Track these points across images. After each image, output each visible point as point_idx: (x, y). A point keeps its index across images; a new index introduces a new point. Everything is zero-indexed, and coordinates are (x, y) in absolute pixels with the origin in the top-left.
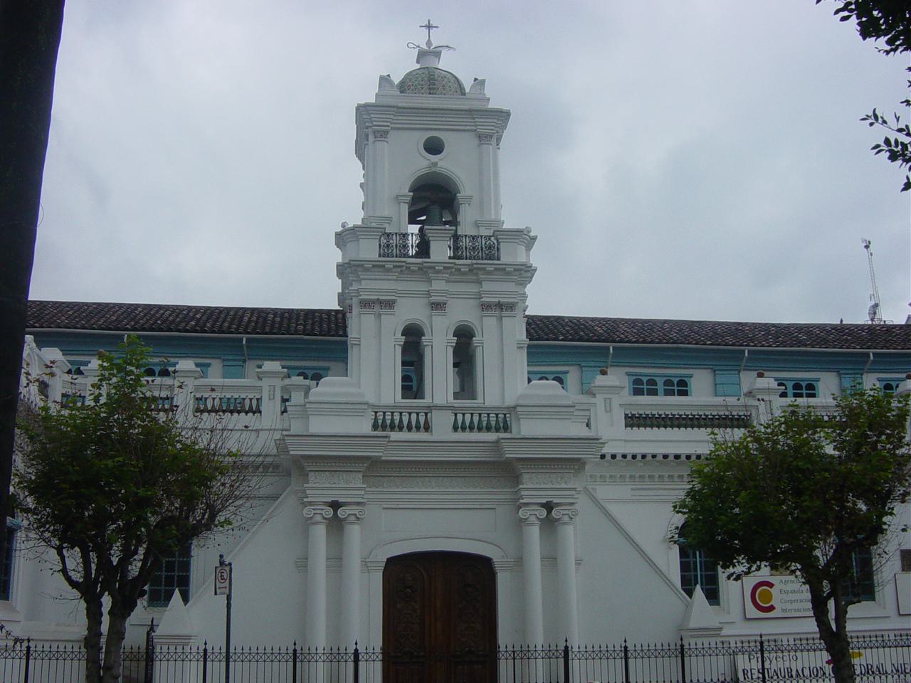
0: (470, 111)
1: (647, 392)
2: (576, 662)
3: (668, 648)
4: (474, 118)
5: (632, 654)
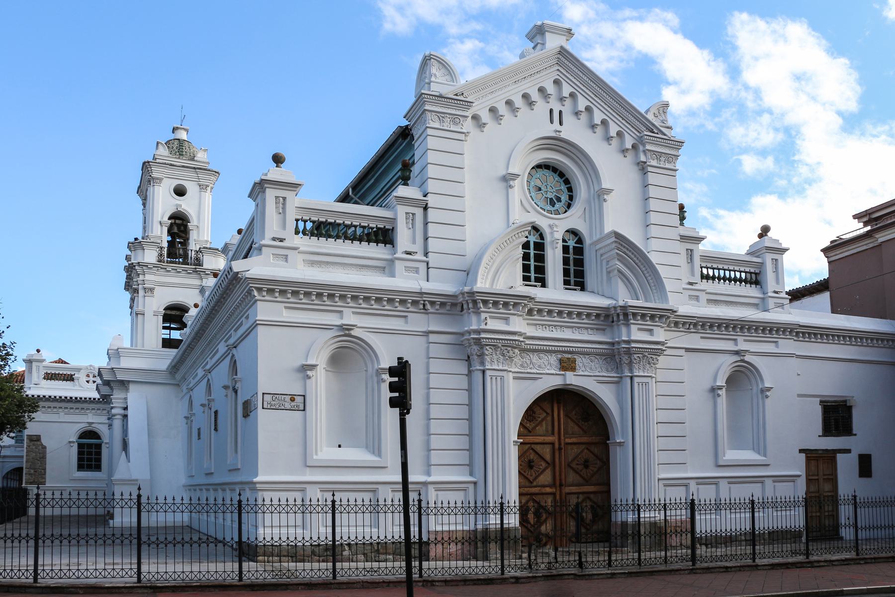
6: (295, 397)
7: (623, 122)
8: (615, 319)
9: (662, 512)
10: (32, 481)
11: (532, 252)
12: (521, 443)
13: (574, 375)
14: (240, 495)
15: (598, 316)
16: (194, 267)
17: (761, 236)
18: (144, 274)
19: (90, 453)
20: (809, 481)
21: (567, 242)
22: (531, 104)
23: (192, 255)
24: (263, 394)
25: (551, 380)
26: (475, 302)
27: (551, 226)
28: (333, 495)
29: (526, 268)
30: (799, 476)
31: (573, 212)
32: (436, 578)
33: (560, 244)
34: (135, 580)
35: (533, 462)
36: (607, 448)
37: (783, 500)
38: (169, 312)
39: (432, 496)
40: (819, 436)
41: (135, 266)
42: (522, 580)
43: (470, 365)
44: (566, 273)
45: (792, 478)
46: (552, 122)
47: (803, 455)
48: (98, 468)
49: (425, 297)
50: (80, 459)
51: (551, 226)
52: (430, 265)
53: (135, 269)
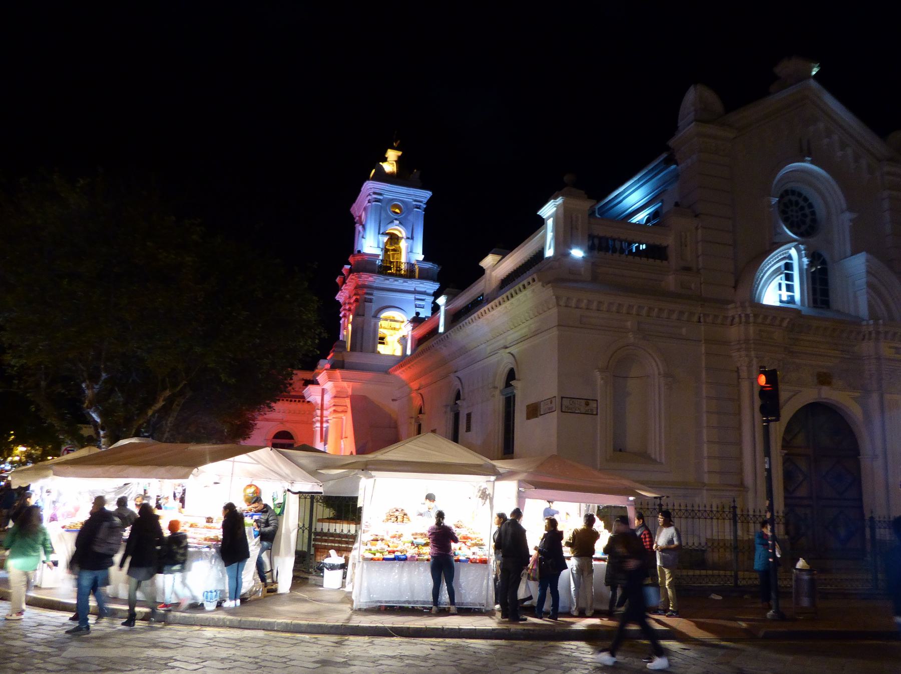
24: (562, 398)
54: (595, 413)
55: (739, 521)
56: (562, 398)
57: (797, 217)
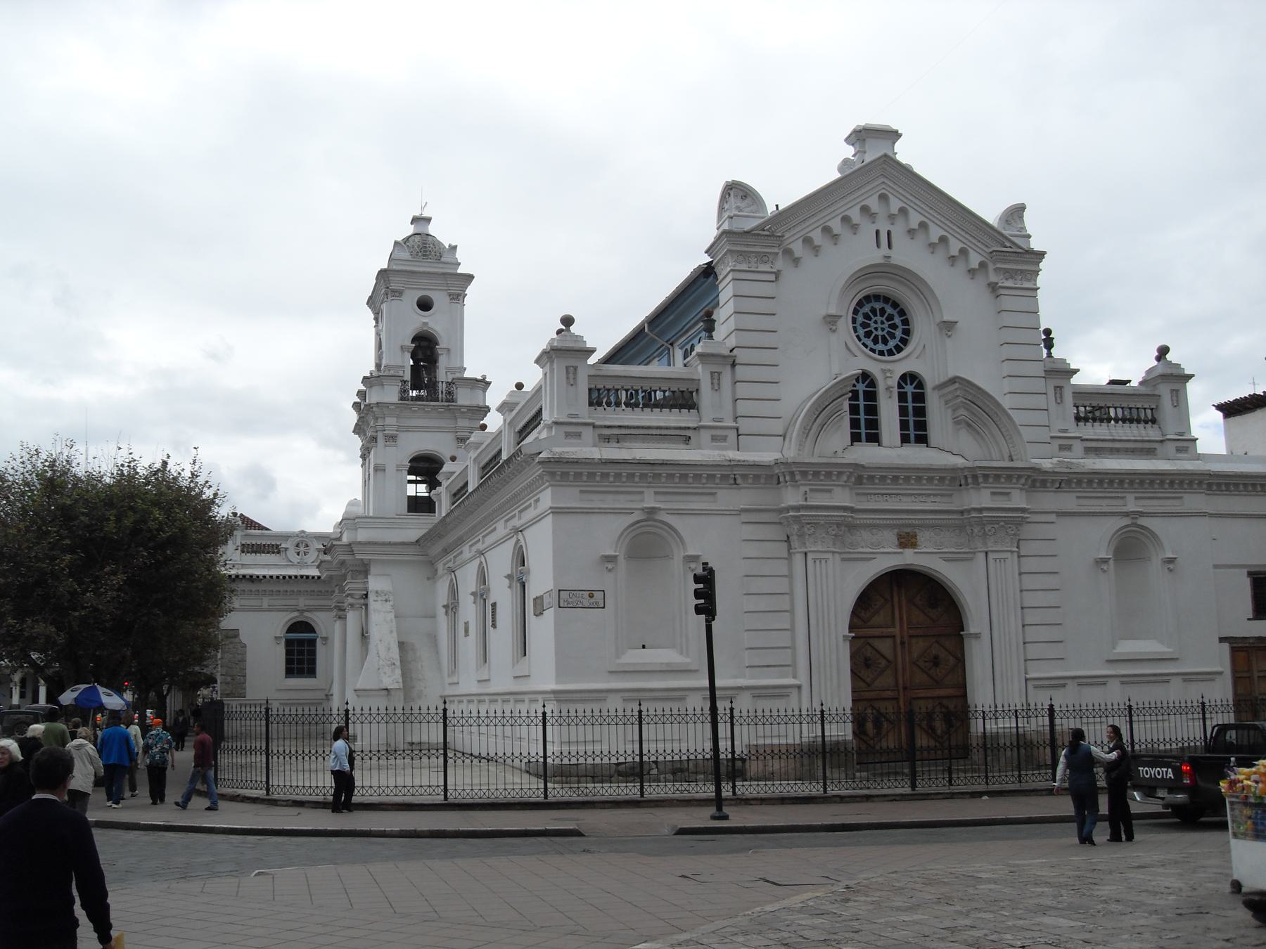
0: (444, 274)
1: (915, 426)
2: (275, 726)
3: (1092, 708)
4: (446, 281)
5: (1135, 712)
6: (593, 592)
7: (967, 236)
8: (963, 482)
9: (1014, 720)
10: (228, 692)
11: (862, 403)
12: (853, 637)
13: (916, 553)
14: (544, 706)
15: (942, 479)
16: (447, 404)
17: (1159, 359)
18: (384, 418)
19: (301, 653)
20: (1237, 680)
21: (904, 388)
22: (854, 228)
23: (442, 387)
24: (559, 590)
25: (890, 559)
26: (792, 474)
27: (884, 371)
28: (640, 705)
29: (855, 424)
30: (1220, 673)
31: (917, 340)
32: (750, 796)
33: (896, 390)
34: (442, 797)
35: (870, 660)
36: (961, 641)
37: (1153, 705)
38: (415, 465)
39: (744, 704)
40: (1249, 619)
41: (372, 408)
42: (846, 799)
43: (790, 547)
44: (904, 425)
45: (1210, 677)
46: (878, 246)
47: (1226, 646)
48: (311, 672)
49: (736, 471)
50: (289, 662)
51: (884, 371)
52: (740, 433)
53: (372, 412)
54: (602, 606)
55: (938, 718)
56: (559, 590)
57: (883, 329)
